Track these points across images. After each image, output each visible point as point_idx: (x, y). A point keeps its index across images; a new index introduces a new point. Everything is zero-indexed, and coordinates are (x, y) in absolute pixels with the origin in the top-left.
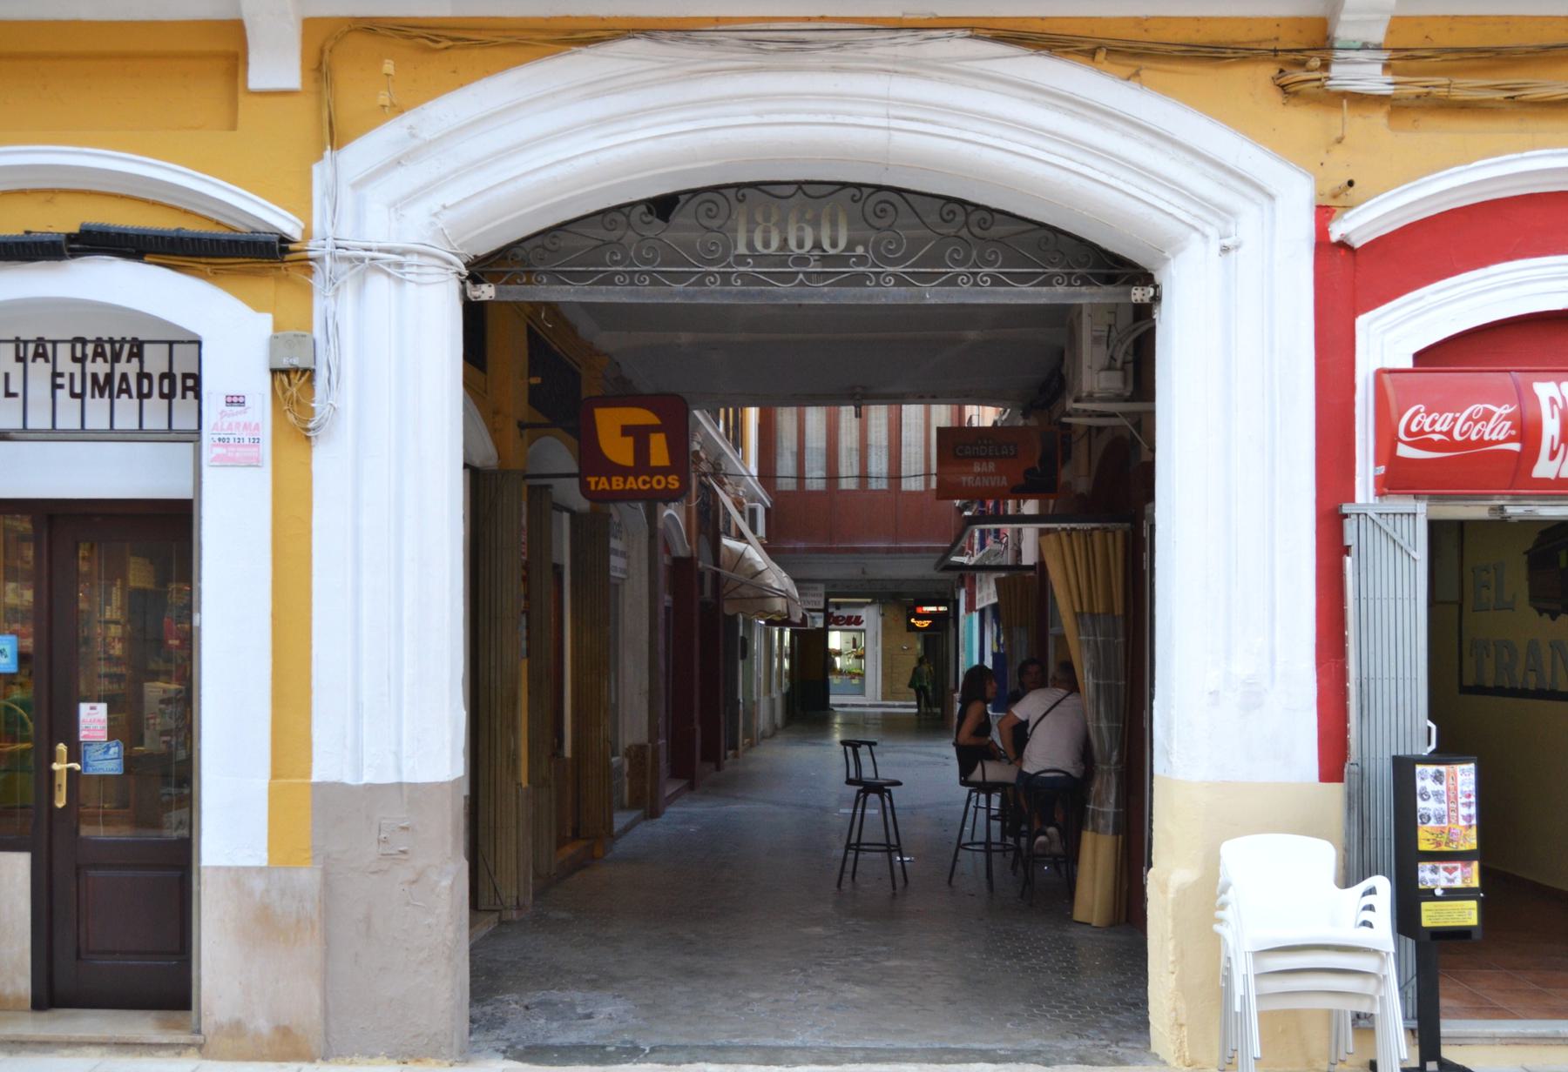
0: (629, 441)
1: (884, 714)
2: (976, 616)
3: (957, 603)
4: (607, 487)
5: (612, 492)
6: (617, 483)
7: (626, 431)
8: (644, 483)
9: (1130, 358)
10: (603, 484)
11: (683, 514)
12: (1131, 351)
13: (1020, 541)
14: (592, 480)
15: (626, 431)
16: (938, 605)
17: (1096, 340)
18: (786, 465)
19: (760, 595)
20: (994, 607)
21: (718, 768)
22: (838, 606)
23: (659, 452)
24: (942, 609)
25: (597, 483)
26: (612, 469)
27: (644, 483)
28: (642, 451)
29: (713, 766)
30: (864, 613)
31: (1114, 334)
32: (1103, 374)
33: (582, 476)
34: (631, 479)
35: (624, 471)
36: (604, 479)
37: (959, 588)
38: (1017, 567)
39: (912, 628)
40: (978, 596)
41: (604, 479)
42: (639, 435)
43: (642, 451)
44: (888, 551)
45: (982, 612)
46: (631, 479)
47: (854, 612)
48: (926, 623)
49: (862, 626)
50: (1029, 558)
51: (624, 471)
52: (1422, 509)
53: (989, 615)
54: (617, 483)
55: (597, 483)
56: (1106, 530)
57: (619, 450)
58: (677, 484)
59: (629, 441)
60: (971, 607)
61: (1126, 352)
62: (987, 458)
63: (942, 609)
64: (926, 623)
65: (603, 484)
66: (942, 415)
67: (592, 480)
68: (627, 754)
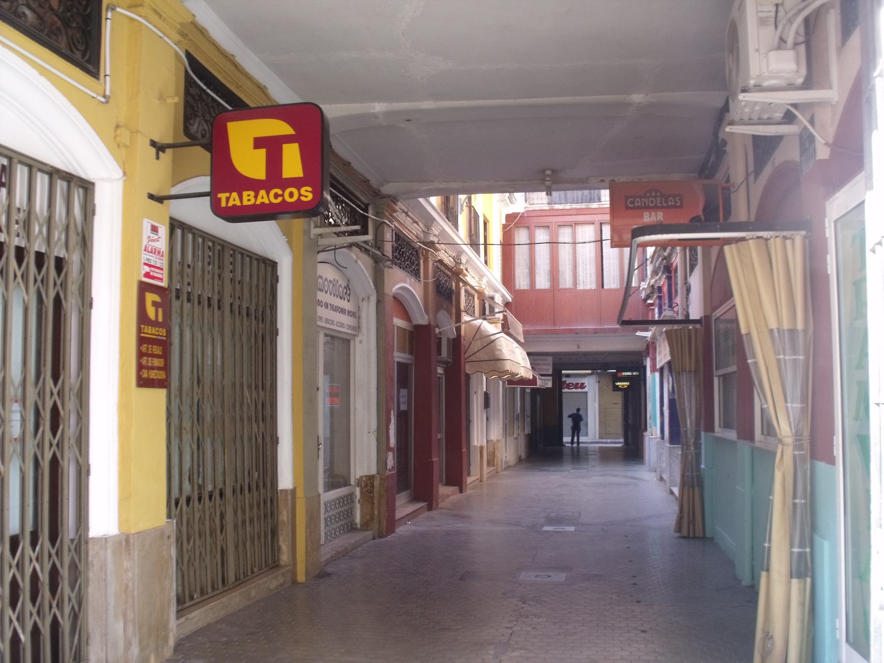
0: (262, 152)
1: (600, 448)
2: (657, 375)
3: (645, 367)
4: (238, 203)
5: (243, 208)
6: (249, 198)
7: (259, 143)
8: (276, 196)
9: (801, 39)
10: (234, 200)
11: (421, 292)
12: (802, 31)
13: (688, 306)
14: (223, 196)
15: (259, 143)
16: (632, 371)
17: (762, 22)
18: (522, 282)
19: (494, 361)
20: (669, 363)
21: (461, 491)
22: (568, 376)
23: (292, 163)
24: (635, 373)
25: (228, 199)
26: (243, 183)
27: (276, 196)
28: (274, 162)
29: (456, 488)
30: (585, 381)
31: (781, 14)
32: (773, 54)
33: (212, 195)
34: (262, 193)
35: (255, 185)
36: (235, 195)
37: (646, 357)
38: (687, 321)
39: (616, 388)
40: (658, 359)
41: (235, 195)
42: (271, 147)
43: (274, 162)
44: (596, 331)
45: (661, 370)
46: (262, 193)
47: (580, 381)
48: (626, 384)
49: (585, 390)
50: (696, 312)
51: (255, 185)
52: (716, 434)
53: (666, 372)
54: (249, 198)
55: (228, 199)
56: (785, 238)
57: (250, 162)
58: (310, 196)
59: (262, 152)
60: (654, 369)
61: (797, 33)
62: (656, 208)
63: (635, 373)
64: (626, 384)
65: (234, 200)
66: (612, 178)
67: (223, 196)
68: (359, 483)
